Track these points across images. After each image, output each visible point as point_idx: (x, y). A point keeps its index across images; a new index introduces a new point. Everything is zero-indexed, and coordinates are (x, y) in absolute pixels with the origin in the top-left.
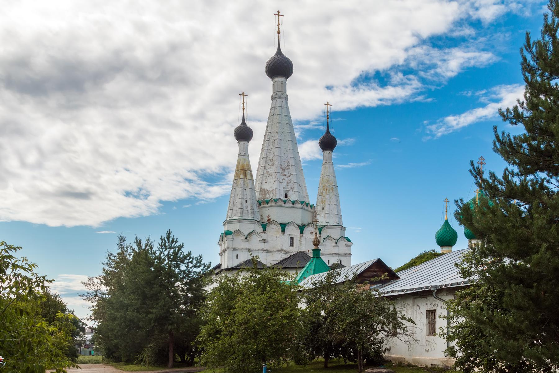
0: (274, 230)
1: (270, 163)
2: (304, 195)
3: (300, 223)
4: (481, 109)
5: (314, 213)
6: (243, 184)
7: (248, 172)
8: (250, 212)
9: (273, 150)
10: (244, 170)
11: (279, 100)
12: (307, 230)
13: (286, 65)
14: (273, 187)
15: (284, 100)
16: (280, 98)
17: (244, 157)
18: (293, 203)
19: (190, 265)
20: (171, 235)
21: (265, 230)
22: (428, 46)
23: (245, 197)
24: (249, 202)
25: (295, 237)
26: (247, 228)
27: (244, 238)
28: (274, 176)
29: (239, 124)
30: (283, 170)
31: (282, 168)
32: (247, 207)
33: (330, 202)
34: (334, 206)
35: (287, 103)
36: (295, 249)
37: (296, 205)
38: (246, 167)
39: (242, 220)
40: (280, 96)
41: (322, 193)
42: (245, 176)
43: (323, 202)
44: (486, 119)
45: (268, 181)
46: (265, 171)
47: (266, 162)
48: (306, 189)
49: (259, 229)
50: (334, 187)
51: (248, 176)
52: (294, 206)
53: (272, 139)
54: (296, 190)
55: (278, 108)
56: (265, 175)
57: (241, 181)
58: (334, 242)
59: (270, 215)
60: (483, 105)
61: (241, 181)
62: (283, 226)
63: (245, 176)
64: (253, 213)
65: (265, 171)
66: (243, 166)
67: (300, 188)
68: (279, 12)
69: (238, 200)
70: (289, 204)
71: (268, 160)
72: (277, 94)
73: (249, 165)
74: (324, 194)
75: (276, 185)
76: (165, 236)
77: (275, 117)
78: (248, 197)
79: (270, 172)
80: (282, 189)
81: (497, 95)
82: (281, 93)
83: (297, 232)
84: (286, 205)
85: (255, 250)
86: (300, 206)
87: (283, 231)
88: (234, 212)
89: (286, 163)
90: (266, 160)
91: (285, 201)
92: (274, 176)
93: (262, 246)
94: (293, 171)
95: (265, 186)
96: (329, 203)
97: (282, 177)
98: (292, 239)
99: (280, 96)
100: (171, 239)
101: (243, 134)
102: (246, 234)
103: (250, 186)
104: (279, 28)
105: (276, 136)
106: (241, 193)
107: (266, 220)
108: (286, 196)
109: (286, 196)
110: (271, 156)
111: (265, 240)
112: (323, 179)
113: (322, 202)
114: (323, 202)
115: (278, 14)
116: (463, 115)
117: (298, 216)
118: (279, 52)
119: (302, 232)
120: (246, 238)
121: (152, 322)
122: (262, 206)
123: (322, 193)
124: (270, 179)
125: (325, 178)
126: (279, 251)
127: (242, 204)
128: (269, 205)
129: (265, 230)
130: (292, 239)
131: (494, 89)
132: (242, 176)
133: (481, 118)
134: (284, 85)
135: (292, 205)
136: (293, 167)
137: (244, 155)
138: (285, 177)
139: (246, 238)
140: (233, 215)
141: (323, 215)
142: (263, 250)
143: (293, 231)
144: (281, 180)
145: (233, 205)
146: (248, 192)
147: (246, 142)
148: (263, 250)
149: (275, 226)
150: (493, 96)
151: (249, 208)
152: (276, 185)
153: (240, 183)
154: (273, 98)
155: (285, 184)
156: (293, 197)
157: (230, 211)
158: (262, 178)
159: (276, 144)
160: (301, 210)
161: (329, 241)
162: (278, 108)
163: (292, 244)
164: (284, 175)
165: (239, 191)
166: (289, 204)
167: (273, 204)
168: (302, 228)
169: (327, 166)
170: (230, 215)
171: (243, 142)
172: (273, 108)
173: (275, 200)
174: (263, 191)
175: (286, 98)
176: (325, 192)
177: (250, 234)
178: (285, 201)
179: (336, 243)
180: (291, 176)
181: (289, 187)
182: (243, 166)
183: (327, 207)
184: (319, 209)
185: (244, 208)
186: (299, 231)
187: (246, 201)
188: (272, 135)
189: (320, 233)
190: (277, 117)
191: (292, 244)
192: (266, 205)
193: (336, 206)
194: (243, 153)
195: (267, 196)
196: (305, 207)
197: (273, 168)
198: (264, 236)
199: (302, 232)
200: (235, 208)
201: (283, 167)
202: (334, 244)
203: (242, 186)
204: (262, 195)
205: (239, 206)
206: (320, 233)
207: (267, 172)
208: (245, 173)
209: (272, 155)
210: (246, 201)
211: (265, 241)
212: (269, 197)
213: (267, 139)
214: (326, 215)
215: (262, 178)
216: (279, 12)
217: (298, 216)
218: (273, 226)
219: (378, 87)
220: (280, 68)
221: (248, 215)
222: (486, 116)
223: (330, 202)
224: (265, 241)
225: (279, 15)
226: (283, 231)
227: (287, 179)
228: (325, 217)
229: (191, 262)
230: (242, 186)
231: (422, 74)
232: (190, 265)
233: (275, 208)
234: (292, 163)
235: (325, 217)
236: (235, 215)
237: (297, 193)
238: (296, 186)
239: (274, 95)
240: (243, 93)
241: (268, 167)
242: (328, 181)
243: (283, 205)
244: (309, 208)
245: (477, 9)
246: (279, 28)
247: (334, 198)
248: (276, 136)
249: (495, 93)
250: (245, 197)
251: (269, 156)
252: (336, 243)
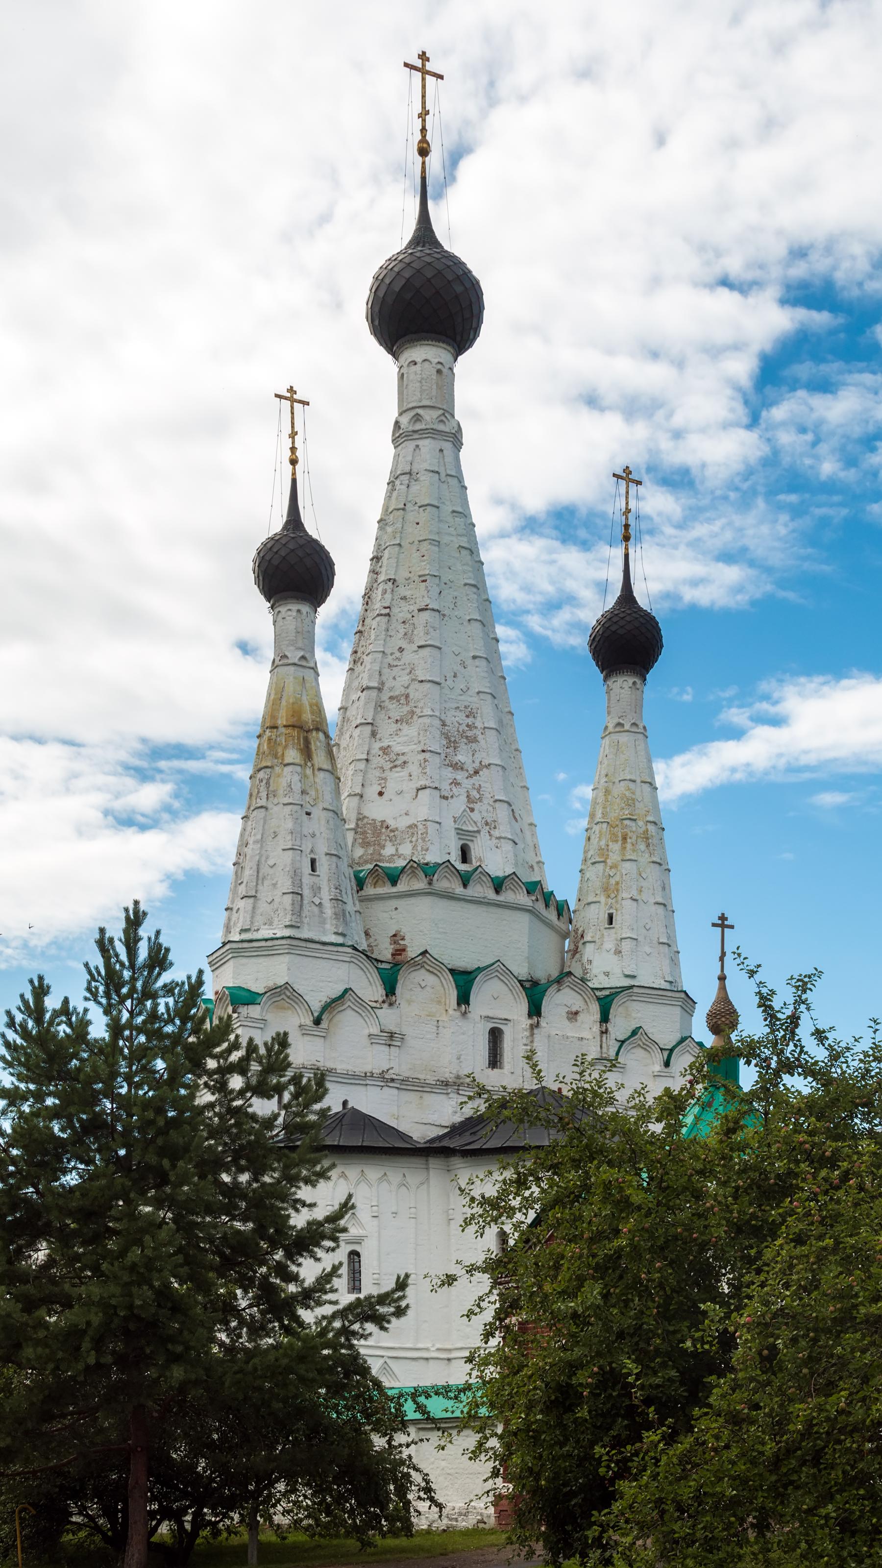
0: (426, 993)
1: (396, 710)
2: (531, 859)
3: (522, 970)
4: (731, 744)
5: (565, 935)
6: (297, 787)
7: (317, 740)
8: (329, 910)
9: (408, 657)
10: (294, 731)
11: (427, 445)
12: (558, 1002)
13: (459, 289)
14: (412, 812)
15: (447, 446)
16: (433, 433)
17: (301, 672)
18: (498, 885)
19: (236, 1082)
20: (145, 932)
21: (390, 990)
22: (547, 537)
23: (307, 846)
24: (324, 866)
25: (507, 1031)
26: (320, 980)
27: (308, 1021)
28: (413, 768)
29: (275, 523)
30: (452, 743)
31: (447, 737)
32: (316, 890)
33: (640, 891)
34: (654, 908)
35: (457, 460)
36: (512, 1077)
37: (507, 896)
38: (308, 717)
39: (298, 944)
40: (429, 428)
41: (604, 852)
42: (307, 752)
43: (610, 890)
44: (751, 774)
45: (392, 787)
46: (377, 745)
47: (379, 706)
48: (533, 835)
49: (370, 988)
50: (651, 828)
51: (320, 758)
52: (501, 898)
53: (401, 612)
54: (504, 829)
55: (425, 478)
56: (376, 761)
57: (288, 777)
58: (658, 1059)
59: (405, 931)
60: (736, 734)
61: (288, 777)
62: (465, 982)
63: (307, 752)
64: (341, 916)
65: (377, 745)
66: (296, 711)
67: (517, 826)
68: (423, 56)
69: (280, 859)
70: (481, 890)
71: (385, 696)
72: (417, 418)
73: (318, 709)
74: (614, 858)
75: (423, 808)
76: (116, 931)
77: (411, 517)
78: (322, 848)
79: (397, 749)
80: (449, 825)
81: (776, 703)
82: (435, 414)
83: (516, 1008)
84: (470, 892)
85: (354, 1076)
86: (523, 899)
87: (464, 999)
88: (263, 906)
89: (461, 717)
90: (378, 696)
91: (458, 875)
92: (413, 768)
93: (377, 1059)
94: (489, 750)
95: (377, 810)
96: (634, 893)
97: (449, 773)
98: (495, 1036)
99: (429, 428)
100: (143, 953)
101: (293, 570)
102: (316, 1007)
103: (327, 799)
104: (423, 130)
105: (421, 595)
106: (290, 825)
107: (385, 952)
108: (465, 856)
109: (465, 856)
110: (398, 682)
111: (392, 1035)
112: (607, 792)
113: (606, 889)
114: (610, 890)
115: (421, 66)
116: (678, 760)
117: (511, 941)
118: (424, 234)
119: (535, 1011)
120: (317, 1022)
121: (86, 1345)
122: (369, 890)
123: (604, 852)
124: (396, 780)
125: (620, 789)
126: (446, 1084)
127: (296, 875)
128: (402, 887)
129: (390, 990)
130: (495, 1036)
131: (764, 686)
132: (292, 755)
133: (734, 770)
134: (444, 378)
135: (491, 895)
136: (491, 735)
137: (294, 662)
138: (460, 776)
139: (317, 1022)
140: (259, 920)
141: (609, 945)
142: (385, 1079)
143: (499, 1001)
144: (445, 786)
145: (259, 878)
146: (319, 823)
147: (305, 608)
148: (385, 1079)
149: (431, 979)
150: (765, 706)
151: (326, 895)
152: (423, 808)
153: (283, 782)
154: (400, 436)
155: (459, 805)
156: (494, 860)
157: (241, 904)
158: (365, 773)
159: (420, 631)
160: (525, 918)
161: (640, 1052)
162: (425, 478)
163: (495, 1061)
164: (457, 767)
165: (282, 819)
166: (481, 890)
167: (420, 884)
168: (534, 994)
169: (624, 738)
170: (241, 920)
171: (294, 607)
172: (401, 477)
173: (429, 871)
174: (372, 832)
175: (456, 438)
176: (616, 847)
177: (333, 1005)
178: (458, 875)
179: (667, 1064)
180: (484, 773)
181: (476, 816)
182: (296, 711)
183: (626, 914)
184: (591, 918)
185: (306, 892)
186: (523, 1006)
187: (313, 862)
188: (402, 591)
189: (605, 1018)
190: (424, 516)
191: (495, 1061)
192: (387, 889)
193: (660, 909)
194: (294, 656)
195: (389, 850)
196: (540, 906)
197: (410, 731)
198: (388, 1017)
199: (535, 1011)
200: (265, 893)
201: (452, 729)
202: (658, 1067)
203: (296, 798)
204: (365, 844)
205: (286, 884)
206: (605, 1018)
207: (385, 750)
208: (307, 742)
209: (405, 679)
210: (313, 862)
211: (391, 1038)
212: (397, 854)
213: (377, 605)
214: (626, 946)
215: (365, 773)
216: (423, 56)
217: (511, 941)
218: (421, 976)
219: (655, 516)
220: (427, 306)
221: (323, 922)
222: (748, 765)
223: (640, 891)
224: (391, 1038)
225: (424, 72)
226: (464, 999)
227: (467, 784)
228: (618, 952)
229: (241, 1068)
230: (296, 798)
231: (535, 622)
232: (236, 1082)
233: (427, 901)
234: (487, 717)
235: (618, 952)
236: (269, 923)
237: (508, 847)
238: (503, 813)
239: (405, 420)
240: (291, 390)
241: (386, 728)
242: (630, 802)
243: (459, 890)
244: (551, 915)
245: (678, 435)
246: (423, 130)
247: (652, 873)
248: (421, 595)
249: (766, 697)
250: (307, 846)
251: (389, 683)
252: (667, 1064)
